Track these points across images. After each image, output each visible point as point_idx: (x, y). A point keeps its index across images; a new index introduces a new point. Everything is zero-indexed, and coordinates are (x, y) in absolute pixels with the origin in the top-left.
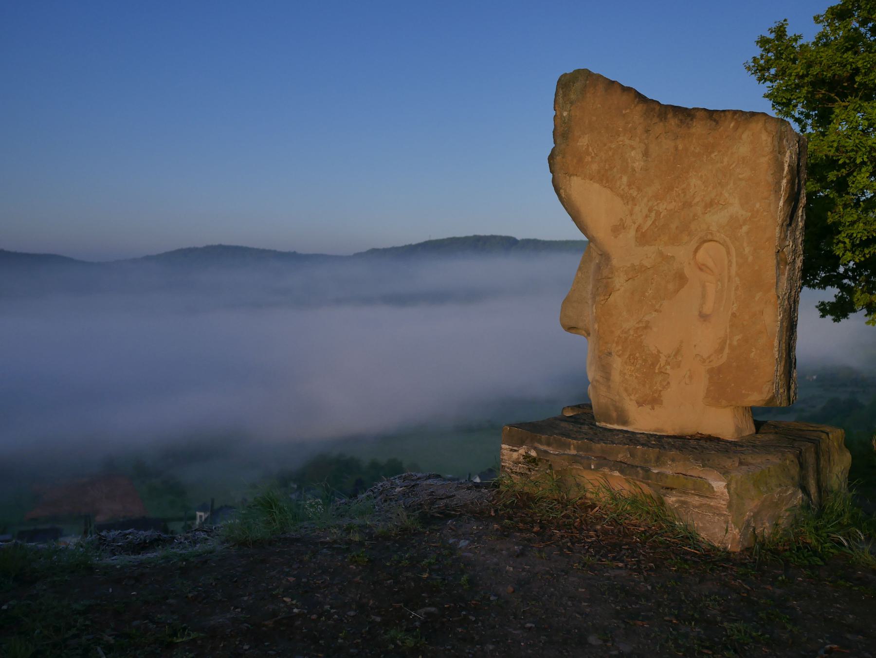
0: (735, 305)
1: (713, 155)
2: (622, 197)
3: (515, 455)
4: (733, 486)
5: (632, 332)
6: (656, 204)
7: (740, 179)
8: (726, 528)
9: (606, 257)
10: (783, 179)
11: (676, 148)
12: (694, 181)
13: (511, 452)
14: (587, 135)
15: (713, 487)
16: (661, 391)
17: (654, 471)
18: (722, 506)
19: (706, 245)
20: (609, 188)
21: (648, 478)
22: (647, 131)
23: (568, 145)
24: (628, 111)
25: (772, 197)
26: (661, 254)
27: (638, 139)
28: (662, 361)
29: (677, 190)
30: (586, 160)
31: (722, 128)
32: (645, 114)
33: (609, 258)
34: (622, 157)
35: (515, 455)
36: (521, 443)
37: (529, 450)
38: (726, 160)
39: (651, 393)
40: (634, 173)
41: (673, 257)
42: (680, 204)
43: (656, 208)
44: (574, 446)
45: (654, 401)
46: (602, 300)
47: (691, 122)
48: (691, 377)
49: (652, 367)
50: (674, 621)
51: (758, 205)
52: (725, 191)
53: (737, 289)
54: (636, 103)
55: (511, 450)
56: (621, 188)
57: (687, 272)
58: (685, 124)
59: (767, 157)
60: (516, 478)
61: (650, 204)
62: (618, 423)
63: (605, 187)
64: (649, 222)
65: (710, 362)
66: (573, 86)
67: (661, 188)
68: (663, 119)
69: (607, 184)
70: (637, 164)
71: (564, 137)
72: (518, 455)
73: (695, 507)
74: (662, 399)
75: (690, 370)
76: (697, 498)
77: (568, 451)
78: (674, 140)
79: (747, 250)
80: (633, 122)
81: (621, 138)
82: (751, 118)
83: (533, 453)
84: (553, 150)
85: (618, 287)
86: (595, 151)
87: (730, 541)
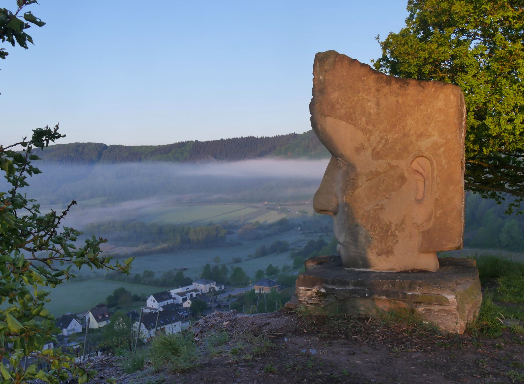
0: (438, 193)
1: (421, 107)
2: (362, 130)
3: (309, 293)
4: (459, 297)
5: (372, 212)
6: (385, 134)
7: (439, 121)
8: (456, 322)
9: (351, 167)
10: (463, 122)
11: (398, 102)
12: (410, 121)
13: (306, 291)
14: (338, 92)
15: (448, 299)
16: (392, 246)
17: (409, 294)
18: (454, 309)
19: (418, 159)
20: (353, 124)
21: (406, 298)
22: (378, 91)
23: (324, 97)
24: (365, 78)
25: (458, 131)
26: (389, 164)
27: (372, 95)
28: (393, 227)
29: (399, 126)
30: (337, 107)
31: (427, 91)
32: (376, 80)
33: (355, 167)
34: (362, 106)
35: (309, 293)
36: (313, 285)
37: (320, 288)
38: (429, 109)
39: (386, 248)
40: (370, 116)
41: (397, 166)
42: (401, 135)
43: (385, 137)
44: (351, 283)
45: (389, 252)
46: (350, 193)
47: (407, 87)
48: (410, 237)
49: (386, 232)
50: (478, 376)
51: (449, 136)
52: (429, 128)
53: (438, 184)
54: (371, 74)
55: (307, 290)
56: (362, 125)
57: (406, 175)
58: (403, 88)
59: (454, 109)
60: (310, 307)
61: (381, 134)
62: (363, 267)
63: (351, 124)
64: (381, 146)
65: (422, 227)
66: (327, 61)
67: (388, 125)
68: (389, 84)
69: (352, 122)
70: (372, 110)
71: (321, 92)
72: (312, 293)
73: (435, 312)
74: (393, 250)
75: (410, 232)
76: (437, 306)
77: (348, 287)
78: (397, 96)
79: (444, 162)
80: (369, 85)
81: (361, 94)
82: (444, 86)
83: (323, 291)
84: (312, 100)
85: (360, 185)
86: (343, 102)
87: (459, 328)
